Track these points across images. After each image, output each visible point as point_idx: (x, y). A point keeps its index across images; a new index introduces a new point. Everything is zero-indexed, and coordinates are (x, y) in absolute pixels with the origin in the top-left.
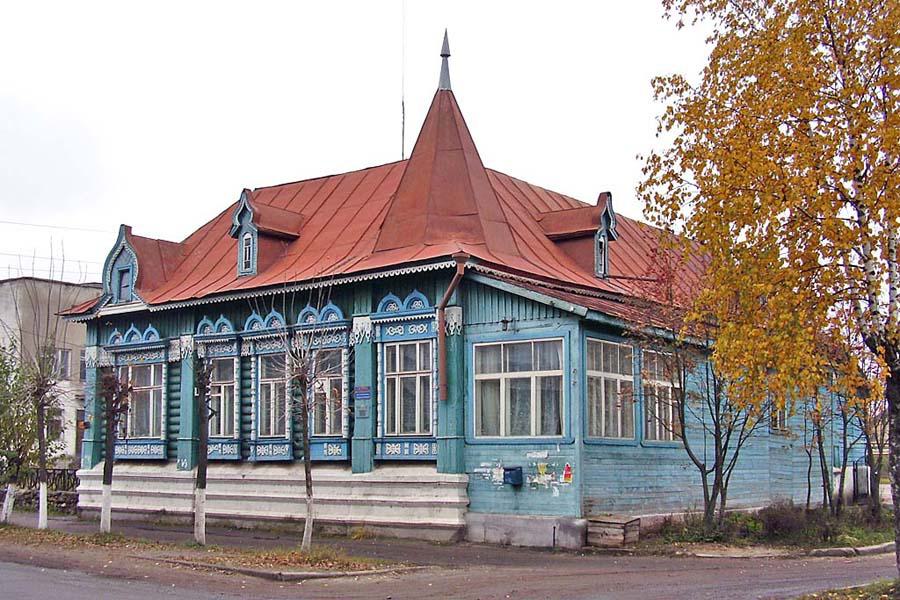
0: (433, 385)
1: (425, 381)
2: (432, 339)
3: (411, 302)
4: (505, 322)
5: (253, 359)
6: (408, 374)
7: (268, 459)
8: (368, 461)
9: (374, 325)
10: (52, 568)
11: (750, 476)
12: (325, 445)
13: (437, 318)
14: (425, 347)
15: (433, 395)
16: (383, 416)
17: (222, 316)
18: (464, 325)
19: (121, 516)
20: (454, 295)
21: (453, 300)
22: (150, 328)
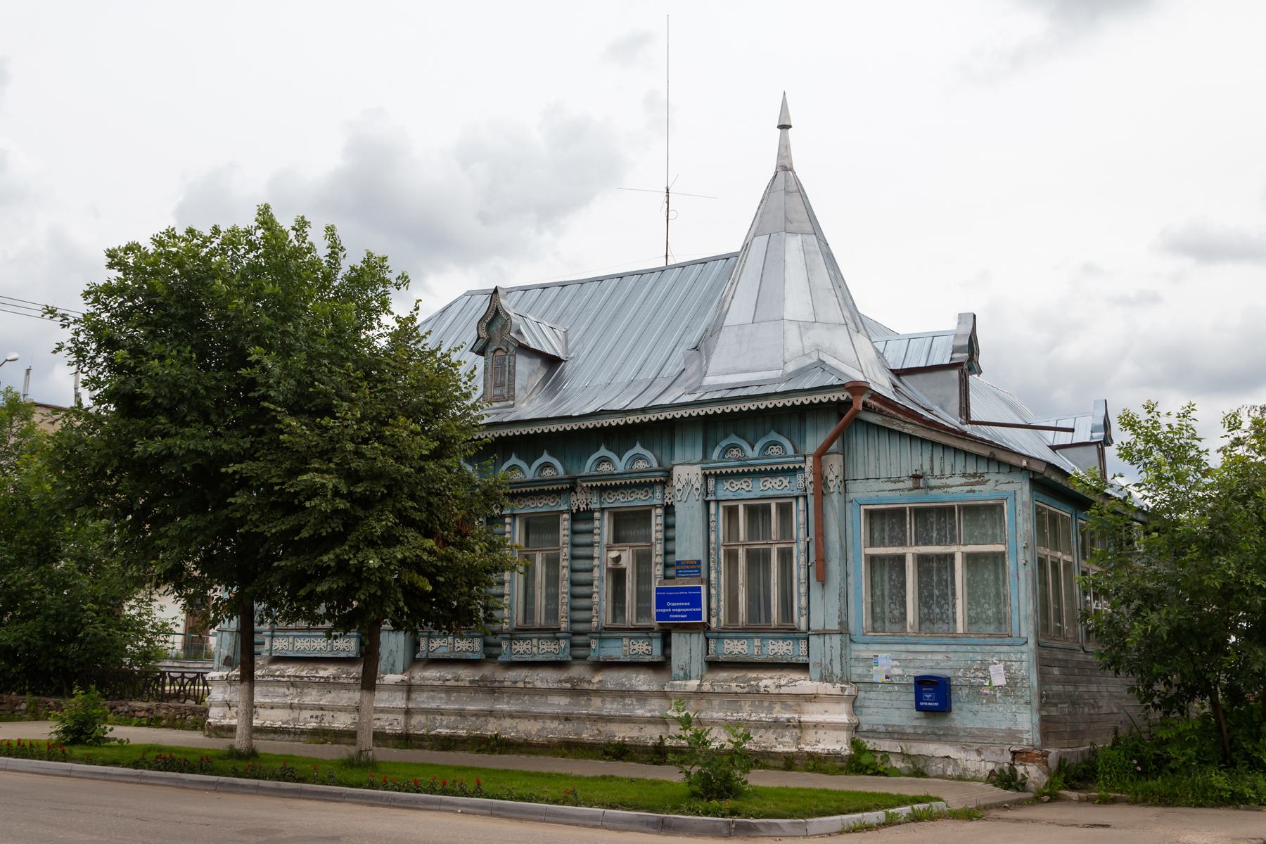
0: (798, 560)
1: (786, 556)
2: (797, 498)
3: (765, 448)
4: (916, 477)
5: (508, 520)
6: (759, 545)
7: (529, 658)
8: (697, 666)
9: (706, 477)
10: (604, 778)
11: (812, 714)
12: (535, 641)
13: (807, 469)
14: (785, 510)
15: (798, 571)
16: (719, 601)
17: (638, 445)
18: (845, 481)
19: (229, 735)
20: (835, 444)
21: (834, 447)
22: (546, 457)
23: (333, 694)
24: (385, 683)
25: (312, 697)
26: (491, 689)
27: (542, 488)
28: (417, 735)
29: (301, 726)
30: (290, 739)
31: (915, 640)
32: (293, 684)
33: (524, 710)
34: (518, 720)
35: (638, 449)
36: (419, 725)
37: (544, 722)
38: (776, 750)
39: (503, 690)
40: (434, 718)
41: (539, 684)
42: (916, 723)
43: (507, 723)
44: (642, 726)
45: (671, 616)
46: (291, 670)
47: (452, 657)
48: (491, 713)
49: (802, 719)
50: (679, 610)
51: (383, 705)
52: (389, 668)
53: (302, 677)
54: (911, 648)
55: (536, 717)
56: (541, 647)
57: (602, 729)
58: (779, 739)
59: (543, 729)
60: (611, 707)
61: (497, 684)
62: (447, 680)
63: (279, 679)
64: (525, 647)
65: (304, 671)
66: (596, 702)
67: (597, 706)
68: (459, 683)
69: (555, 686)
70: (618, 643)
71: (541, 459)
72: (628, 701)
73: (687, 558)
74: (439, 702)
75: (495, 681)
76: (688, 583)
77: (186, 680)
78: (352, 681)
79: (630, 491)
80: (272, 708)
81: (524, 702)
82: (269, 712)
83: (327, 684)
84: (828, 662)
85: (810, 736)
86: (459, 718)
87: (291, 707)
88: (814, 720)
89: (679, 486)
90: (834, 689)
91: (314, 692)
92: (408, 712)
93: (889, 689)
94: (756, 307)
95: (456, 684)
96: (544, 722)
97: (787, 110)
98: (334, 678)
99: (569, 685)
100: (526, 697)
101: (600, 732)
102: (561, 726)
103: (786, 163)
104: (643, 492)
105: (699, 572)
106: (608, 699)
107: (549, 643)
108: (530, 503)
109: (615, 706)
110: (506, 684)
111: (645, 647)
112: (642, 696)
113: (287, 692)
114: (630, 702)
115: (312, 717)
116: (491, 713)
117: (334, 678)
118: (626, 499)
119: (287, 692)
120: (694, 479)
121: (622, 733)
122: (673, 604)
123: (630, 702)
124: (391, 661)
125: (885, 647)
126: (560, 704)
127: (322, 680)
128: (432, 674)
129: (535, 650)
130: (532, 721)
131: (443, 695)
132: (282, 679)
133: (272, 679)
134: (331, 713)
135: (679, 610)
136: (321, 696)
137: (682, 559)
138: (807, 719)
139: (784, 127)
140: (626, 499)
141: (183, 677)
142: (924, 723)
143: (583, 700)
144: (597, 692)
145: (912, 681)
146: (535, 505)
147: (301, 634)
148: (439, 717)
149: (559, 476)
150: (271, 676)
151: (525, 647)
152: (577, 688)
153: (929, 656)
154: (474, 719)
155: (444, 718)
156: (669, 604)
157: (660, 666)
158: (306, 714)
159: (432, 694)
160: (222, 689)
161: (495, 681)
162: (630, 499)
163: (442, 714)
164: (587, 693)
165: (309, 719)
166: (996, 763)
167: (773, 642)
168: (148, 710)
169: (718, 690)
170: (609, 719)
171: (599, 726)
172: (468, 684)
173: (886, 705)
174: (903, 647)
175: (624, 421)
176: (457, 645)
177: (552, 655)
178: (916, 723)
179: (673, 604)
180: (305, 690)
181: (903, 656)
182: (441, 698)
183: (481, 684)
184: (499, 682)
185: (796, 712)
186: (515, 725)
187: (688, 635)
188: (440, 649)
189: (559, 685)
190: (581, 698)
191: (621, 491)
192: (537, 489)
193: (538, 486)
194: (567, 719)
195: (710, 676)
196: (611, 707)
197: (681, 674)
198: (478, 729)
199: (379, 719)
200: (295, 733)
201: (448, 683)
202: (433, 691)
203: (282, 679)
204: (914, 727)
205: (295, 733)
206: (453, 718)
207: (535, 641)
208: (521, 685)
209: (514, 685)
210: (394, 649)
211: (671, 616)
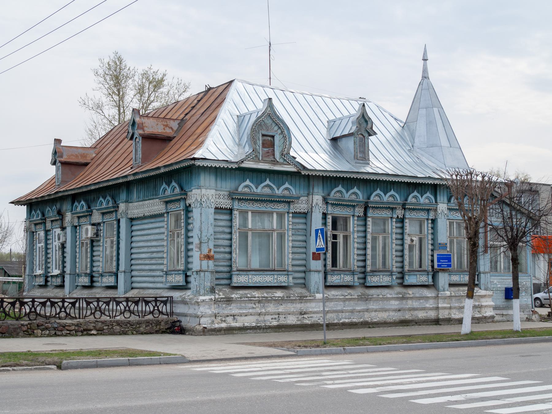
12: (276, 277)
23: (284, 306)
24: (316, 298)
25: (271, 308)
26: (365, 299)
27: (389, 206)
28: (334, 323)
29: (268, 324)
30: (261, 331)
31: (504, 275)
32: (259, 302)
33: (383, 307)
34: (378, 312)
35: (355, 190)
36: (332, 318)
37: (389, 313)
38: (475, 316)
39: (372, 299)
40: (338, 314)
41: (389, 296)
42: (503, 304)
43: (373, 314)
44: (427, 311)
45: (442, 266)
46: (256, 294)
47: (344, 285)
48: (367, 310)
49: (482, 304)
50: (445, 263)
51: (316, 310)
52: (316, 290)
53: (267, 297)
54: (502, 278)
55: (386, 310)
56: (384, 279)
57: (413, 314)
58: (475, 312)
59: (389, 315)
60: (416, 304)
61: (370, 297)
62: (346, 296)
63: (252, 299)
64: (377, 279)
65: (265, 294)
66: (410, 302)
67: (410, 304)
68: (353, 297)
69: (396, 296)
70: (415, 277)
71: (285, 185)
72: (421, 301)
73: (442, 242)
74: (340, 306)
75: (369, 295)
76: (444, 253)
77: (66, 304)
78: (298, 298)
79: (419, 212)
80: (246, 316)
81: (380, 304)
82: (243, 318)
83: (279, 301)
84: (486, 283)
85: (483, 310)
86: (350, 314)
87: (259, 314)
88: (485, 304)
89: (439, 212)
90: (490, 293)
91: (272, 305)
92: (437, 308)
93: (497, 292)
94: (449, 141)
95: (351, 297)
96: (389, 313)
97: (426, 51)
98: (287, 297)
99: (401, 296)
100: (381, 302)
101: (412, 315)
102: (396, 314)
103: (426, 75)
104: (349, 209)
105: (447, 248)
106: (414, 301)
107: (387, 277)
108: (378, 212)
109: (417, 304)
110: (374, 296)
111: (425, 279)
112: (427, 298)
113: (254, 306)
114: (422, 302)
115: (272, 319)
116: (367, 310)
117: (287, 297)
118: (417, 215)
119: (254, 306)
120: (444, 210)
121: (421, 315)
122: (443, 261)
123: (422, 302)
124: (317, 287)
125: (495, 278)
126: (395, 304)
127: (280, 298)
128: (333, 293)
129: (381, 280)
130: (384, 312)
131: (342, 303)
132: (254, 299)
133: (247, 299)
134: (284, 316)
135: (445, 263)
136: (276, 307)
137: (440, 242)
138: (484, 304)
139: (425, 60)
140: (417, 215)
141: (33, 301)
142: (505, 303)
143: (404, 302)
144: (411, 298)
145: (504, 289)
146: (381, 213)
147: (258, 273)
148: (340, 314)
149: (398, 202)
150: (246, 297)
151: (259, 279)
152: (405, 296)
153: (507, 280)
154: (358, 313)
155: (343, 314)
156: (441, 261)
157: (434, 286)
158: (268, 318)
159: (336, 303)
160: (208, 307)
161: (369, 295)
162: (419, 215)
163: (343, 312)
164: (408, 298)
165: (271, 320)
166: (528, 315)
167: (254, 276)
168: (77, 325)
169: (457, 295)
170: (414, 309)
171: (411, 312)
172: (357, 297)
173: (496, 298)
174: (500, 278)
175: (369, 177)
176: (345, 278)
177: (350, 282)
178: (503, 304)
179: (443, 261)
180: (266, 305)
181: (500, 281)
182: (341, 305)
183: (363, 296)
184: (371, 295)
185: (480, 302)
186: (377, 315)
187: (444, 273)
188: (336, 281)
189: (397, 295)
190: (404, 301)
191: (416, 211)
192: (387, 206)
193: (388, 205)
194: (399, 310)
195: (326, 291)
196: (416, 304)
197: (442, 289)
198: (361, 318)
199: (312, 317)
200: (264, 329)
201: (347, 297)
202: (336, 301)
203: (254, 299)
204: (503, 305)
205: (266, 329)
206: (347, 314)
207: (381, 277)
208: (381, 296)
209: (378, 297)
210: (318, 281)
211: (442, 266)
